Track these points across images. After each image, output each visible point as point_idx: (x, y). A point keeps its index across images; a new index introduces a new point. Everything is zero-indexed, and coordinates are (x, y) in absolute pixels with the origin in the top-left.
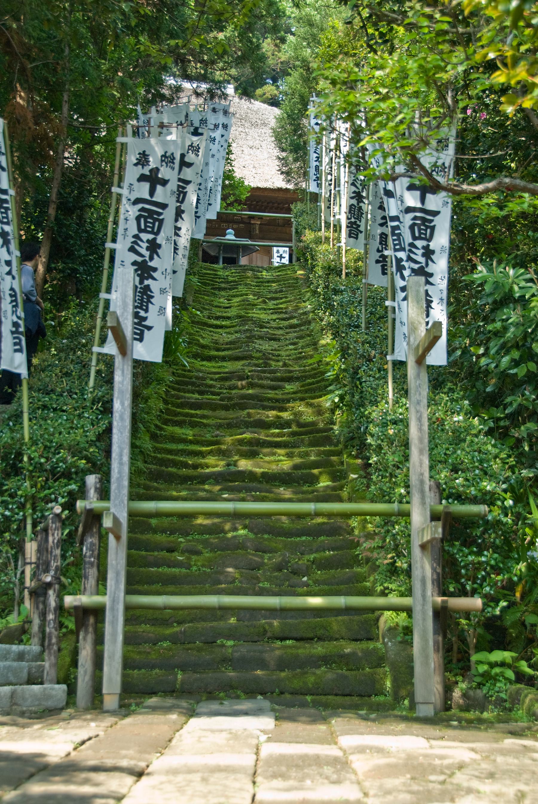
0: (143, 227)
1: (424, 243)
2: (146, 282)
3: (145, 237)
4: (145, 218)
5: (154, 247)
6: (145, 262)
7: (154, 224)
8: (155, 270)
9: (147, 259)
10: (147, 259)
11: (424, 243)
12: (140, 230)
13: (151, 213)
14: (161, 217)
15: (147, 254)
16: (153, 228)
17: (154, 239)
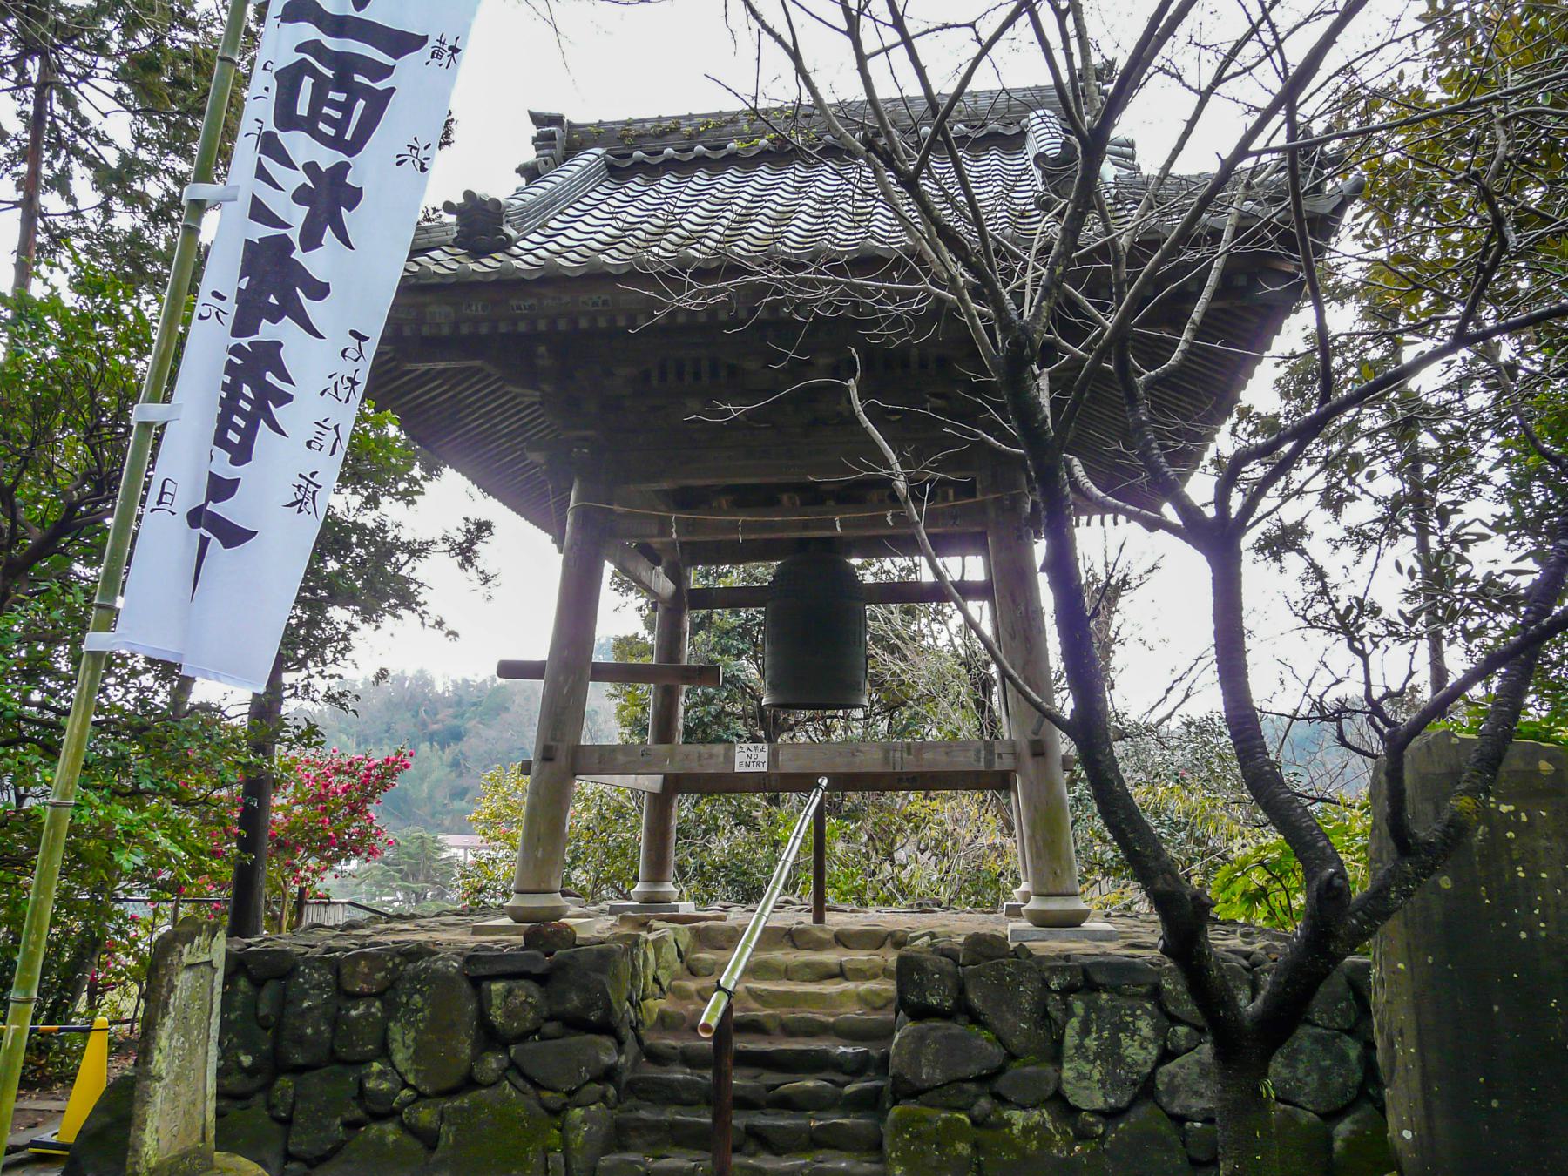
0: (302, 109)
1: (327, 158)
2: (267, 331)
3: (300, 145)
4: (320, 86)
5: (331, 199)
6: (284, 245)
7: (346, 108)
8: (320, 291)
9: (294, 235)
10: (294, 235)
11: (327, 158)
12: (286, 117)
13: (345, 64)
14: (380, 86)
15: (297, 215)
16: (341, 126)
17: (343, 168)
